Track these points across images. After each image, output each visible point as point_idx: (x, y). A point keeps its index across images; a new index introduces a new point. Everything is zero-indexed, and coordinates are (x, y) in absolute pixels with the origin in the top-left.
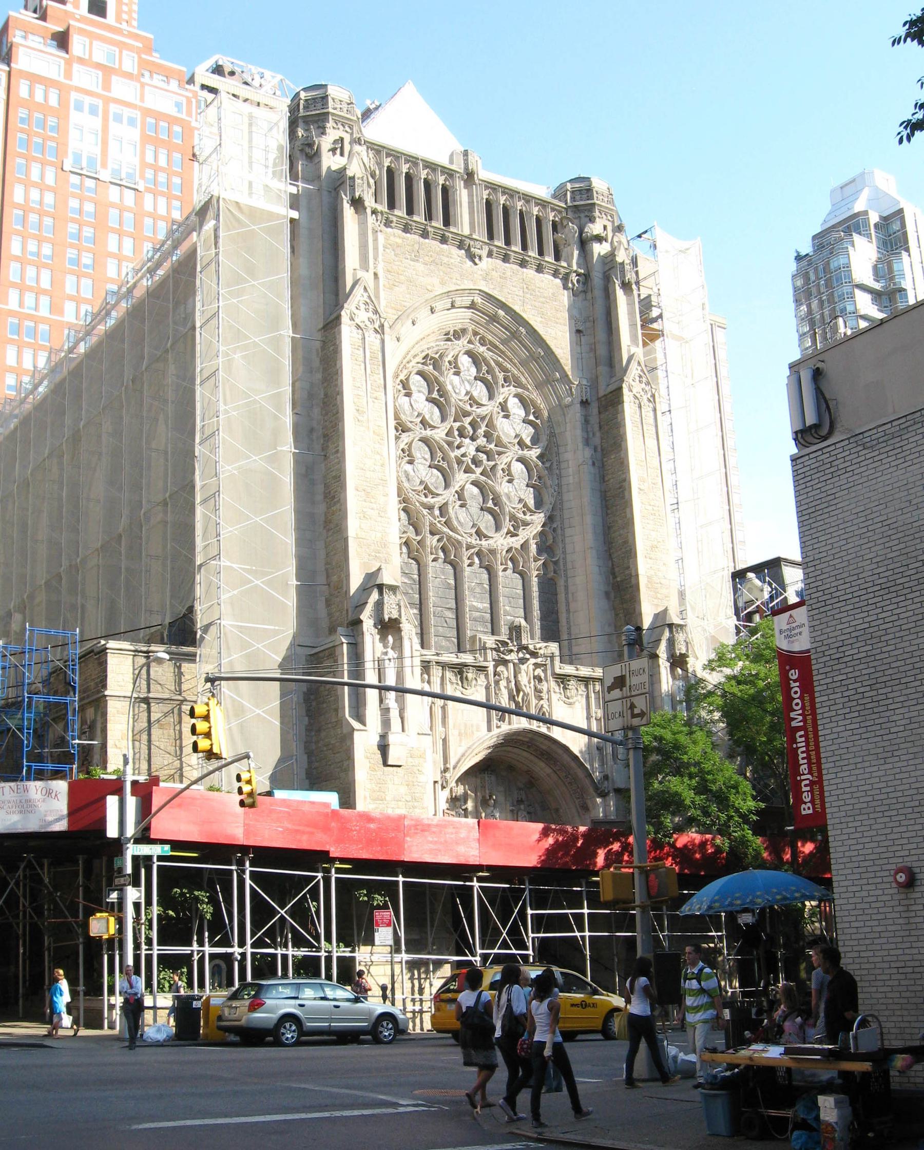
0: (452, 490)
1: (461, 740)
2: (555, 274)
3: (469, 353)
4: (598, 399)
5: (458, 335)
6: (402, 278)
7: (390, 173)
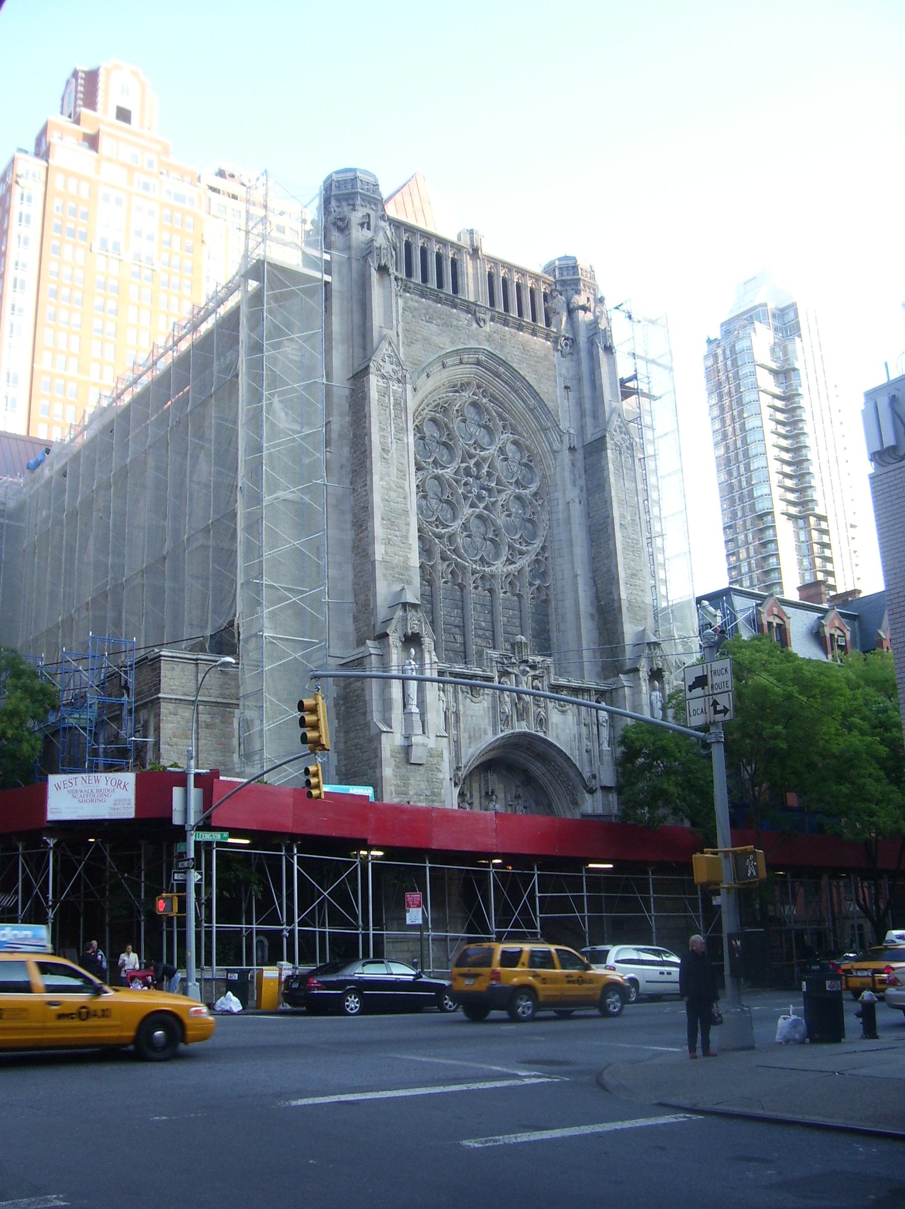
0: (459, 522)
1: (470, 743)
2: (547, 337)
3: (474, 404)
4: (584, 446)
5: (464, 386)
6: (419, 336)
7: (408, 246)
